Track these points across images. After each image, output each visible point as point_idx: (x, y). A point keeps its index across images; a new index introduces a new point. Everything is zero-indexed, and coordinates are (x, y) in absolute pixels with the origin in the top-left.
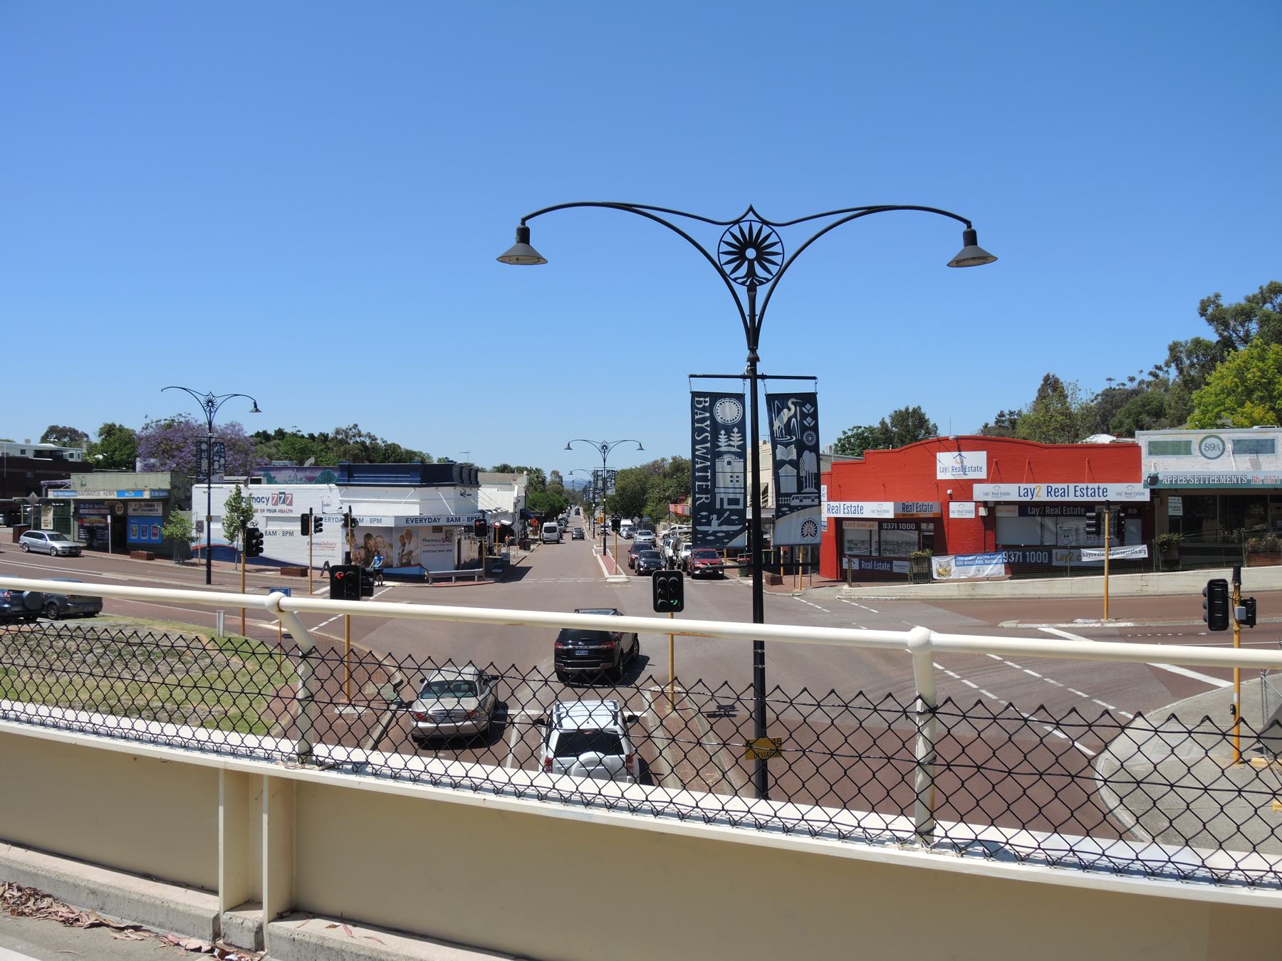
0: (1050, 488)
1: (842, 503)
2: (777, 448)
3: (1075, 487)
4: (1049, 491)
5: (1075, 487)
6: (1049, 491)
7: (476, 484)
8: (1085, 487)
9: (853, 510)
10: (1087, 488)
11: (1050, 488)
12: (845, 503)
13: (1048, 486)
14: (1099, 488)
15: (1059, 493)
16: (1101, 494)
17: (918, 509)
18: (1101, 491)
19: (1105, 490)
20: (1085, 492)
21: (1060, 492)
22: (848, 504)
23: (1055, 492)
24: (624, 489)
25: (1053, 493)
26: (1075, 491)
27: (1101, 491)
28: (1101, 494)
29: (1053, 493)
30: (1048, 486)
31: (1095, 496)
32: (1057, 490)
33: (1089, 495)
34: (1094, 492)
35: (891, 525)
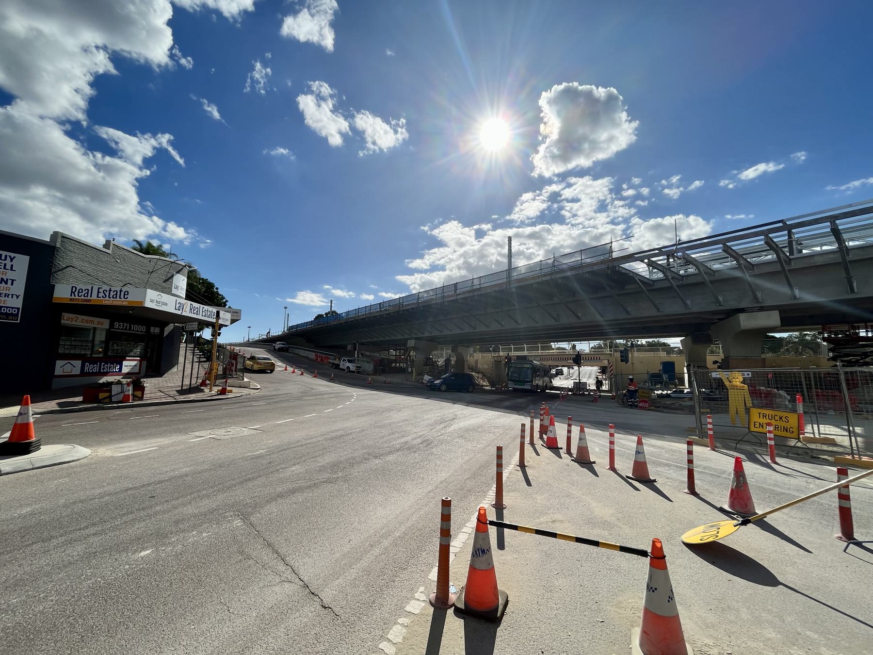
0: (74, 288)
1: (202, 306)
2: (596, 178)
3: (99, 288)
4: (74, 291)
5: (99, 288)
6: (74, 291)
7: (692, 445)
8: (108, 289)
9: (209, 314)
10: (110, 290)
11: (74, 288)
12: (204, 306)
13: (73, 287)
14: (121, 291)
15: (83, 294)
16: (122, 296)
17: (204, 313)
18: (123, 293)
19: (126, 293)
20: (107, 294)
21: (84, 292)
22: (206, 307)
23: (79, 292)
24: (58, 251)
25: (76, 293)
26: (99, 292)
27: (123, 293)
28: (122, 296)
29: (76, 293)
30: (73, 287)
31: (116, 298)
32: (81, 291)
33: (111, 296)
34: (116, 294)
35: (123, 326)
